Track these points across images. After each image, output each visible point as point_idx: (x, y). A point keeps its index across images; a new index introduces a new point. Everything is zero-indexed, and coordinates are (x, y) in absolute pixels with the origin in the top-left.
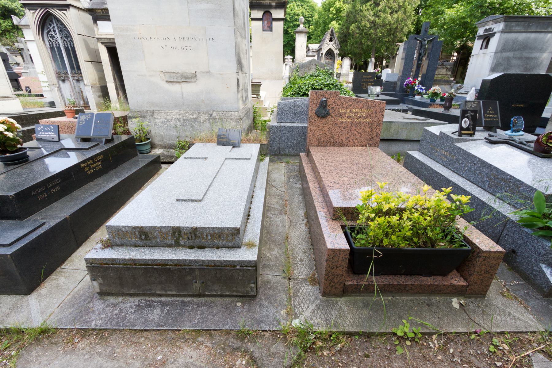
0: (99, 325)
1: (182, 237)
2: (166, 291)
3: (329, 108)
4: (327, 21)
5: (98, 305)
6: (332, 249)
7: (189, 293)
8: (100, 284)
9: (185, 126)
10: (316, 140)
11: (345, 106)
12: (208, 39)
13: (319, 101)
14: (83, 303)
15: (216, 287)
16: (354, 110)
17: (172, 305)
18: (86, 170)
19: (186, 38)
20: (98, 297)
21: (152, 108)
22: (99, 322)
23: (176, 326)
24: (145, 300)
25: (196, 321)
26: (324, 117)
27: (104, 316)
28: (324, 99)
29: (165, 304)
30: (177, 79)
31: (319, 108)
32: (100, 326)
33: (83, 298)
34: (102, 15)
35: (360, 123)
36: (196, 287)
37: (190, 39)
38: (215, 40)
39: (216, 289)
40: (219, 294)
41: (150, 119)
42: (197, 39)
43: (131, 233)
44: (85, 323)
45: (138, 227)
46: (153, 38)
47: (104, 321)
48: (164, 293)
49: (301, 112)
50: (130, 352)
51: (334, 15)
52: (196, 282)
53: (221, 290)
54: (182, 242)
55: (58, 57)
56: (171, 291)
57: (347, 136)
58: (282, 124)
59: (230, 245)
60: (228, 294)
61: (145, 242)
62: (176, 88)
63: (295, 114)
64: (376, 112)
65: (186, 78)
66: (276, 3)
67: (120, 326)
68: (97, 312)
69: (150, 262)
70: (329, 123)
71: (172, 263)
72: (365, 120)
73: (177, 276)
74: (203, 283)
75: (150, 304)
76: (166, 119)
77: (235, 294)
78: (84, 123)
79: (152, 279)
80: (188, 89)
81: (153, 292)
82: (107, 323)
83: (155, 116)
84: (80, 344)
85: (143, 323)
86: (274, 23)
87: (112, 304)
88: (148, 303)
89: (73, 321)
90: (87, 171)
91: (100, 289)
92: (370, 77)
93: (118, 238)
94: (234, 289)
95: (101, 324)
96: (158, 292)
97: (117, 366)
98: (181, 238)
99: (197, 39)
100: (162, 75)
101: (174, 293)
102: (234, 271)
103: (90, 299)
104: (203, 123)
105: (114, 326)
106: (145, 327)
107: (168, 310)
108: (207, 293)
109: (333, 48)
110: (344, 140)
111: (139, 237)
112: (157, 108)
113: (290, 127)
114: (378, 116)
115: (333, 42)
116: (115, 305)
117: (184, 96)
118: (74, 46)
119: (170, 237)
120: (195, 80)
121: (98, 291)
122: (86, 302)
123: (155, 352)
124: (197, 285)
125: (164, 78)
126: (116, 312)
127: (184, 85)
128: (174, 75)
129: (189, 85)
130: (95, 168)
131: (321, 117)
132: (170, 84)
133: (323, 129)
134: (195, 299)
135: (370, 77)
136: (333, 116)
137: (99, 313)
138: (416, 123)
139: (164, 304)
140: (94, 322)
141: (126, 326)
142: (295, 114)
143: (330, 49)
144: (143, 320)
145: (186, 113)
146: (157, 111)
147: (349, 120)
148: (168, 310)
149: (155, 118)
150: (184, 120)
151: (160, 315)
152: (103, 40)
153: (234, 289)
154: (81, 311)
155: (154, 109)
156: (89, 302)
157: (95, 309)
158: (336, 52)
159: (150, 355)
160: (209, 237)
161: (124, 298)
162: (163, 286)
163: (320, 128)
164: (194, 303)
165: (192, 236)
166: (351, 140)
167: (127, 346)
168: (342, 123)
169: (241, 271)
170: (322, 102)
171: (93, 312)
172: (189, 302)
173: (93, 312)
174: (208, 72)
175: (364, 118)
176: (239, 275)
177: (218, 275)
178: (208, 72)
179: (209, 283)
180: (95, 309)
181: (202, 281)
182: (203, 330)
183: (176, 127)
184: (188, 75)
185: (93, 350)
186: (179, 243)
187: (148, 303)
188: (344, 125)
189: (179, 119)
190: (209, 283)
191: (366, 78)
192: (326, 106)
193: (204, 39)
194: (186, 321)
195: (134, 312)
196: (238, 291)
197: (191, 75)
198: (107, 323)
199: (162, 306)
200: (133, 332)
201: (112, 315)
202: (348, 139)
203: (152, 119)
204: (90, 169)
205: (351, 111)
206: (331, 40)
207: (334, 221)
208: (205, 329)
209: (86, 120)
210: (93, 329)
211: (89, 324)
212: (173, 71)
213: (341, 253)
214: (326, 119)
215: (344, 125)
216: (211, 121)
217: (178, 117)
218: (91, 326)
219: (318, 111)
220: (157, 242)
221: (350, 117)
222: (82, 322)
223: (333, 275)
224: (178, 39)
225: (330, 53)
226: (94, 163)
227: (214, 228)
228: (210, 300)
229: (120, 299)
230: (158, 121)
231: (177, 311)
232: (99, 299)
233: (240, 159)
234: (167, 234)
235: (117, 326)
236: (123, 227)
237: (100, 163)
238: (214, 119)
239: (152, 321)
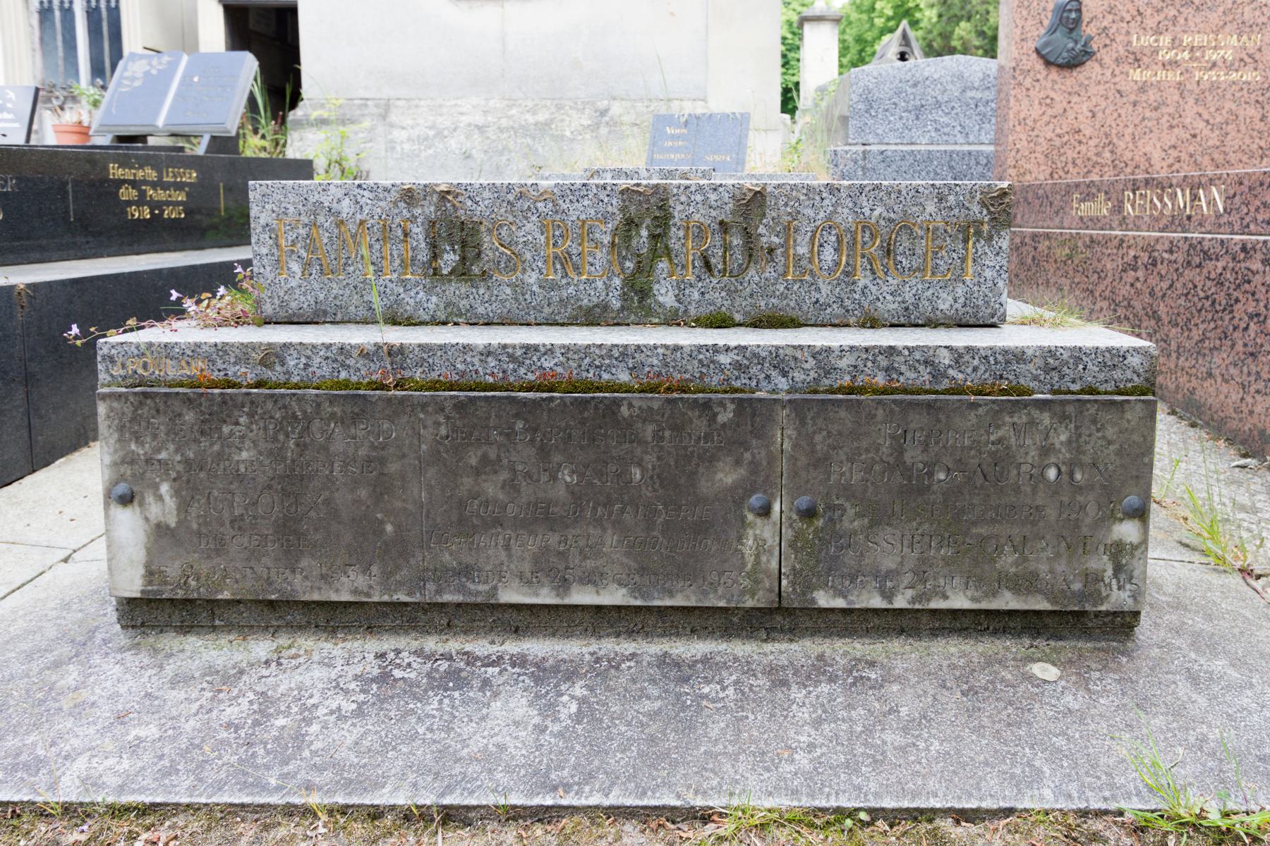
0: (113, 781)
1: (668, 252)
2: (563, 585)
3: (1089, 30)
4: (869, 36)
5: (123, 673)
8: (160, 533)
9: (501, 153)
10: (1041, 158)
11: (1150, 22)
14: (17, 668)
15: (888, 551)
16: (1187, 39)
17: (603, 675)
20: (123, 639)
23: (667, 784)
24: (419, 653)
25: (803, 760)
26: (1072, 63)
29: (556, 669)
31: (1052, 30)
32: (121, 789)
33: (25, 646)
35: (1214, 86)
36: (761, 548)
39: (889, 563)
40: (900, 602)
41: (372, 129)
43: (386, 233)
45: (428, 190)
47: (147, 757)
48: (546, 597)
49: (938, 104)
51: (889, 19)
52: (765, 512)
53: (921, 575)
54: (665, 295)
55: (59, 38)
56: (592, 579)
57: (1169, 139)
59: (944, 304)
60: (960, 601)
61: (456, 289)
63: (919, 111)
67: (264, 788)
68: (105, 712)
70: (1093, 90)
71: (624, 377)
72: (1234, 76)
73: (650, 459)
74: (809, 514)
75: (454, 674)
76: (431, 128)
77: (1008, 601)
78: (137, 84)
79: (492, 488)
81: (478, 590)
82: (172, 770)
83: (393, 117)
85: (422, 770)
87: (210, 670)
88: (444, 666)
90: (129, 203)
91: (150, 574)
93: (307, 265)
94: (1008, 561)
96: (511, 595)
98: (663, 265)
101: (614, 596)
102: (1021, 418)
103: (66, 650)
104: (572, 140)
105: (220, 786)
106: (449, 789)
107: (582, 701)
108: (824, 600)
110: (1156, 155)
111: (424, 255)
116: (226, 679)
118: (117, 7)
119: (601, 256)
121: (133, 586)
122: (42, 662)
124: (764, 531)
126: (231, 713)
130: (160, 205)
131: (1060, 67)
133: (1071, 114)
134: (741, 648)
136: (1107, 60)
137: (121, 718)
139: (542, 672)
140: (81, 764)
141: (309, 787)
142: (919, 111)
144: (423, 754)
145: (510, 107)
146: (401, 103)
147: (1173, 76)
148: (582, 701)
149: (392, 125)
150: (501, 130)
151: (541, 730)
153: (1008, 561)
156: (57, 665)
160: (829, 255)
161: (283, 640)
162: (553, 539)
163: (1058, 109)
164: (748, 667)
165: (726, 247)
166: (1184, 156)
168: (1143, 89)
169: (1064, 418)
172: (706, 660)
173: (80, 710)
175: (1229, 67)
176: (1046, 451)
177: (913, 455)
179: (851, 521)
181: (804, 501)
182: (875, 813)
183: (467, 156)
186: (645, 293)
187: (444, 666)
188: (1152, 95)
189: (480, 129)
190: (851, 521)
192: (1078, 21)
195: (360, 712)
196: (1025, 583)
199: (538, 680)
200: (359, 829)
202: (1174, 153)
203: (380, 129)
204: (141, 201)
205: (1176, 44)
208: (888, 803)
209: (147, 74)
210: (68, 810)
214: (1080, 75)
215: (1152, 95)
216: (604, 131)
217: (479, 119)
218: (53, 787)
219: (1046, 44)
220: (519, 288)
221: (1174, 64)
228: (840, 650)
229: (261, 647)
230: (403, 135)
231: (648, 706)
232: (121, 650)
234: (586, 231)
235: (244, 786)
237: (192, 176)
238: (614, 124)
239: (488, 759)
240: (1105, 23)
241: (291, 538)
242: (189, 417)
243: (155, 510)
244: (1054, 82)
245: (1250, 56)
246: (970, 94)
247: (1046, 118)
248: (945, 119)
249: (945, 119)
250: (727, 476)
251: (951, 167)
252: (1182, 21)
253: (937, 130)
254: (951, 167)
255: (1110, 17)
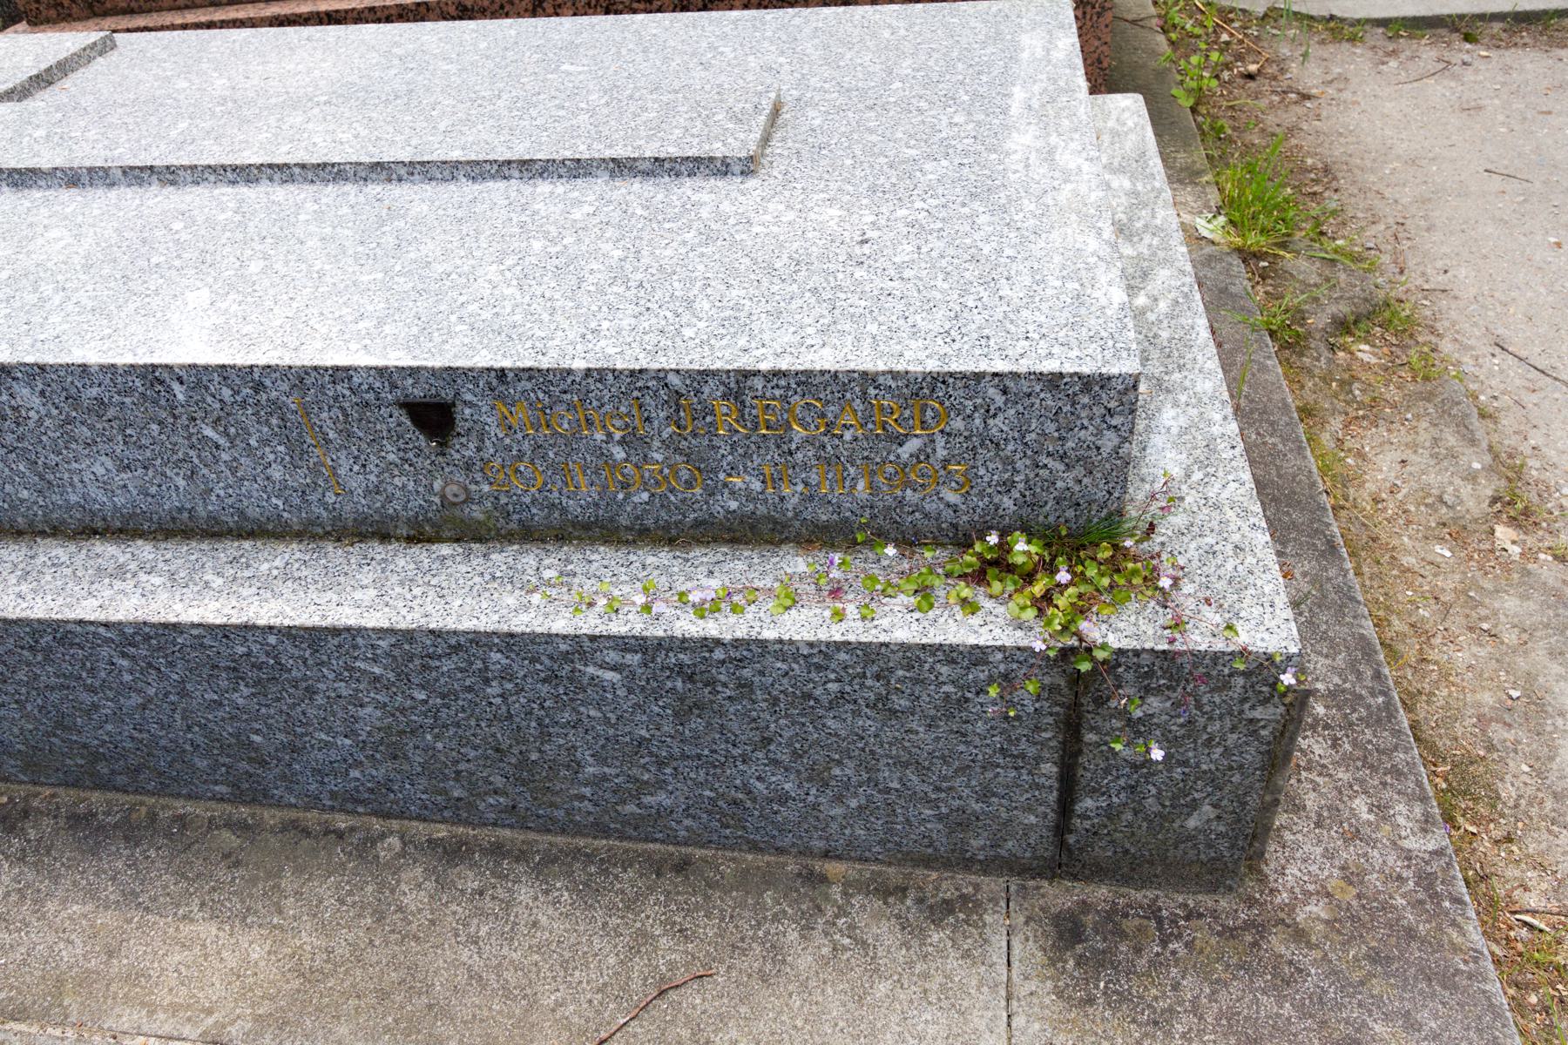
0: (1418, 810)
22: (1404, 815)
27: (1361, 805)
32: (1424, 799)
44: (1435, 896)
47: (1387, 794)
50: (1464, 654)
67: (1388, 704)
68: (1348, 854)
82: (1397, 772)
84: (1532, 901)
89: (1448, 980)
95: (1411, 799)
97: (1556, 669)
123: (1428, 571)
140: (1412, 843)
154: (1375, 957)
157: (1331, 875)
159: (1448, 583)
167: (1445, 675)
171: (1351, 876)
180: (1331, 875)
185: (1534, 811)
194: (1278, 468)
198: (1397, 772)
201: (1346, 761)
211: (1434, 867)
218: (1439, 853)
222: (1441, 912)
232: (1263, 879)
235: (1391, 716)
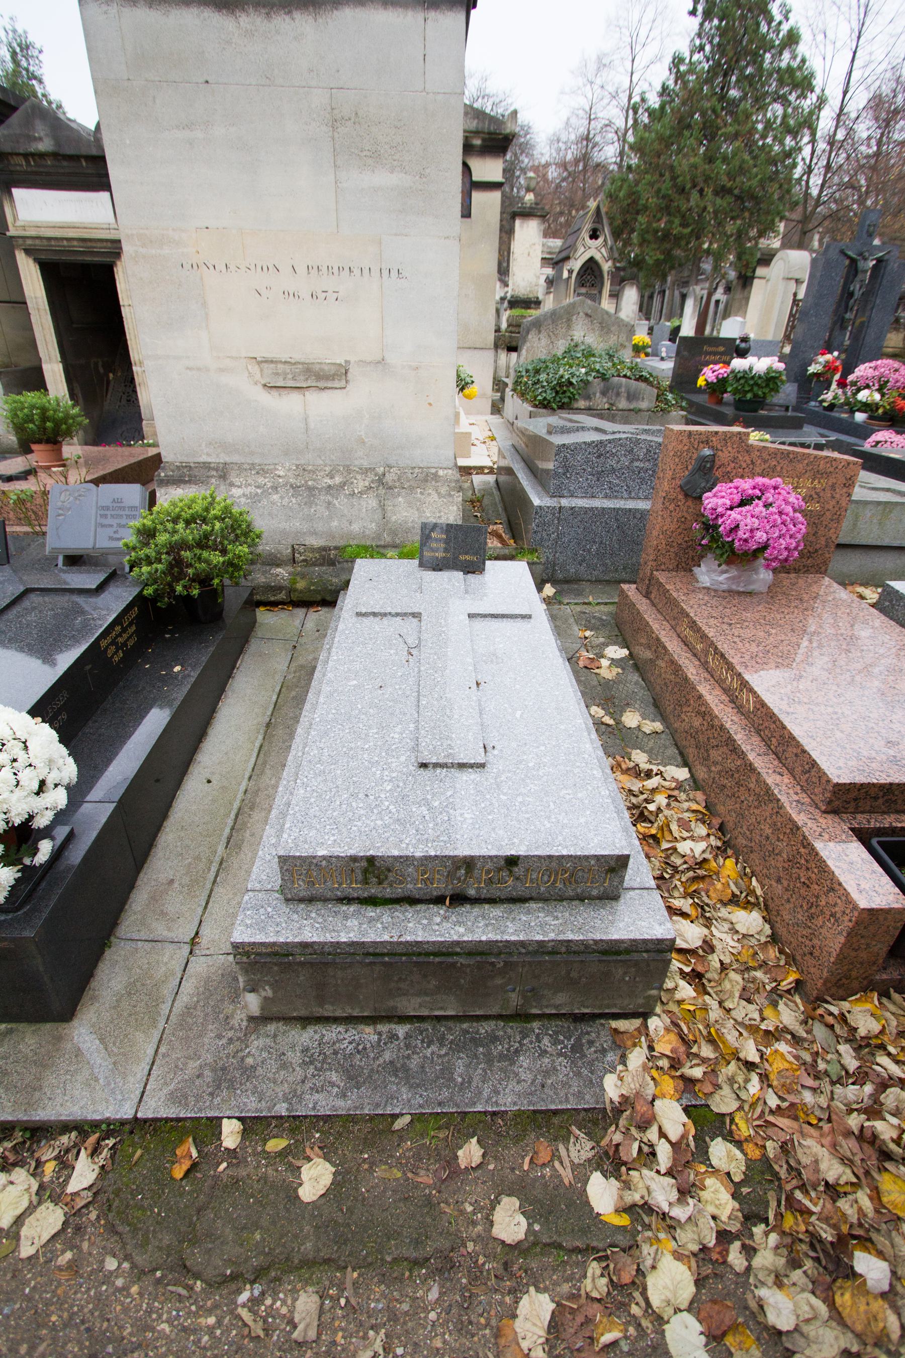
6: (871, 911)
7: (490, 1013)
12: (385, 273)
13: (695, 456)
18: (110, 653)
19: (325, 269)
21: (223, 458)
28: (707, 452)
30: (294, 379)
31: (692, 474)
34: (26, 172)
37: (336, 270)
38: (404, 274)
42: (357, 272)
46: (232, 267)
49: (613, 470)
58: (565, 502)
62: (291, 403)
63: (599, 475)
64: (833, 487)
65: (319, 376)
66: (484, 140)
69: (399, 950)
71: (458, 950)
80: (323, 407)
86: (477, 197)
90: (112, 657)
92: (721, 349)
99: (357, 272)
100: (255, 369)
109: (598, 257)
112: (235, 458)
113: (586, 510)
114: (838, 496)
115: (601, 240)
117: (312, 425)
120: (343, 384)
125: (258, 376)
127: (312, 397)
128: (287, 368)
129: (325, 397)
130: (125, 644)
132: (275, 393)
135: (721, 349)
138: (897, 503)
143: (591, 260)
152: (29, 242)
155: (228, 459)
158: (606, 266)
170: (704, 459)
174: (381, 362)
178: (381, 362)
184: (326, 368)
191: (710, 353)
193: (375, 272)
197: (333, 369)
206: (594, 236)
207: (829, 817)
212: (284, 357)
213: (889, 917)
223: (852, 963)
224: (302, 270)
225: (591, 268)
226: (124, 630)
227: (563, 857)
233: (503, 616)
236: (324, 858)
237: (134, 628)
240: (729, 469)
241: (321, 1000)
242: (276, 968)
243: (263, 994)
244: (689, 507)
245: (817, 494)
246: (637, 464)
247: (679, 530)
248: (617, 481)
249: (617, 481)
250: (499, 981)
251: (617, 520)
252: (779, 469)
253: (610, 488)
254: (617, 520)
255: (733, 465)
